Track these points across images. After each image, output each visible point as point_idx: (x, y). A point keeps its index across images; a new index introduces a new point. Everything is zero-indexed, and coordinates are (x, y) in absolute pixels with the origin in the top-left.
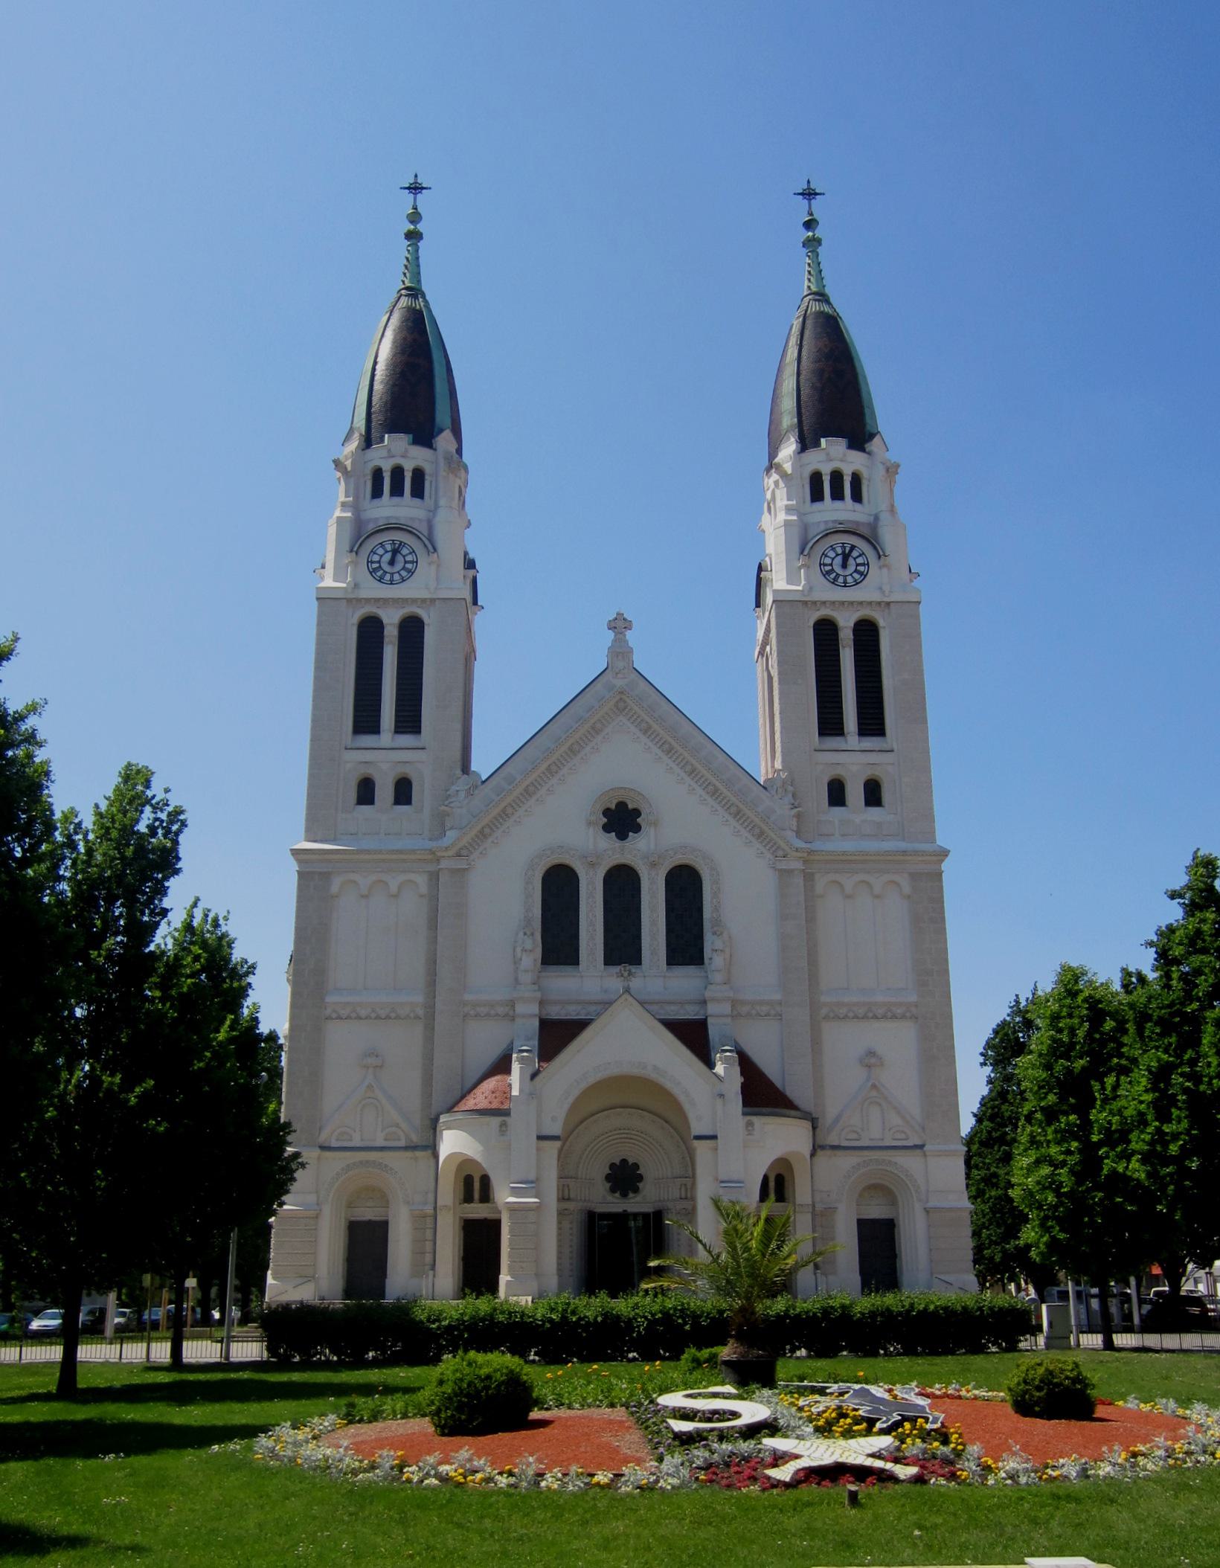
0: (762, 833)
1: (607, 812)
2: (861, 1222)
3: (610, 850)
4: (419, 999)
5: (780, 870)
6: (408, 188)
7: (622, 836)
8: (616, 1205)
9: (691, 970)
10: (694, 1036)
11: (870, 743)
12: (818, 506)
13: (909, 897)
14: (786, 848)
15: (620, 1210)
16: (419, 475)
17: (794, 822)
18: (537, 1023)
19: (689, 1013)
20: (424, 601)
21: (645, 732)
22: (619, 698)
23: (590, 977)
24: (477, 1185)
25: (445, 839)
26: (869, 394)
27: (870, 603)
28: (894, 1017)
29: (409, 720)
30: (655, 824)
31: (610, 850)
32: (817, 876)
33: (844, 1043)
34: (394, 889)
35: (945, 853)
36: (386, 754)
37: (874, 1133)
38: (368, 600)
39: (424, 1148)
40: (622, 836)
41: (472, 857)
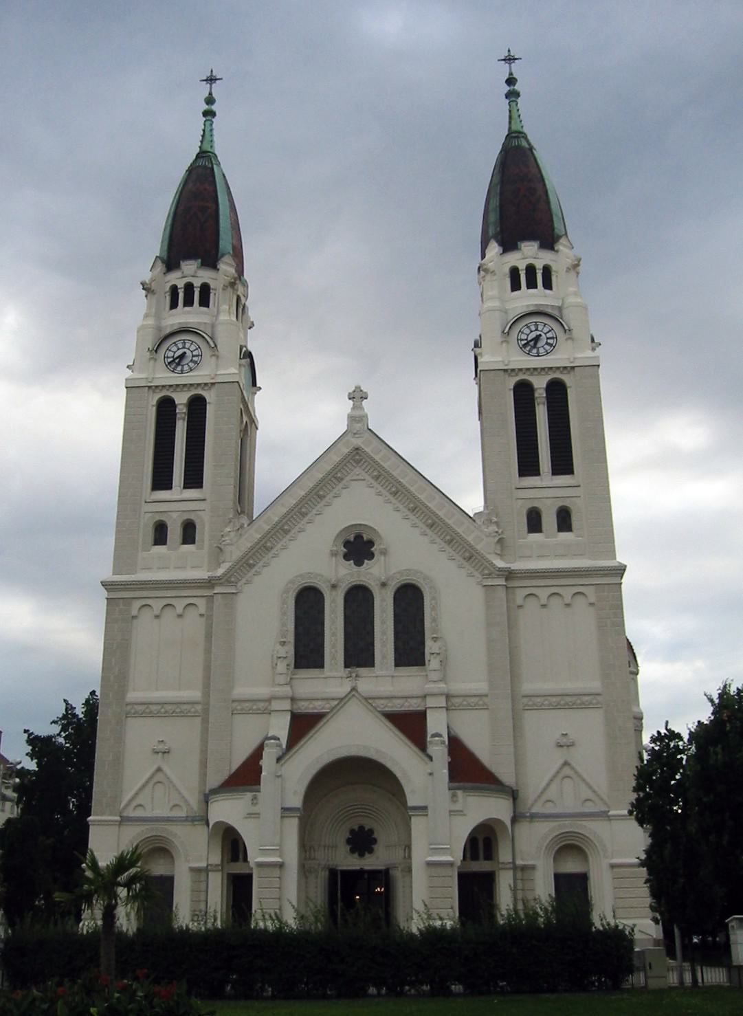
1: (347, 544)
3: (348, 574)
6: (216, 79)
7: (359, 563)
8: (353, 863)
9: (413, 670)
10: (411, 725)
15: (358, 868)
16: (547, 271)
18: (288, 717)
19: (414, 705)
22: (357, 456)
23: (329, 682)
29: (194, 478)
30: (384, 553)
31: (348, 574)
33: (543, 728)
34: (179, 610)
36: (177, 501)
37: (569, 804)
40: (359, 563)
41: (239, 584)
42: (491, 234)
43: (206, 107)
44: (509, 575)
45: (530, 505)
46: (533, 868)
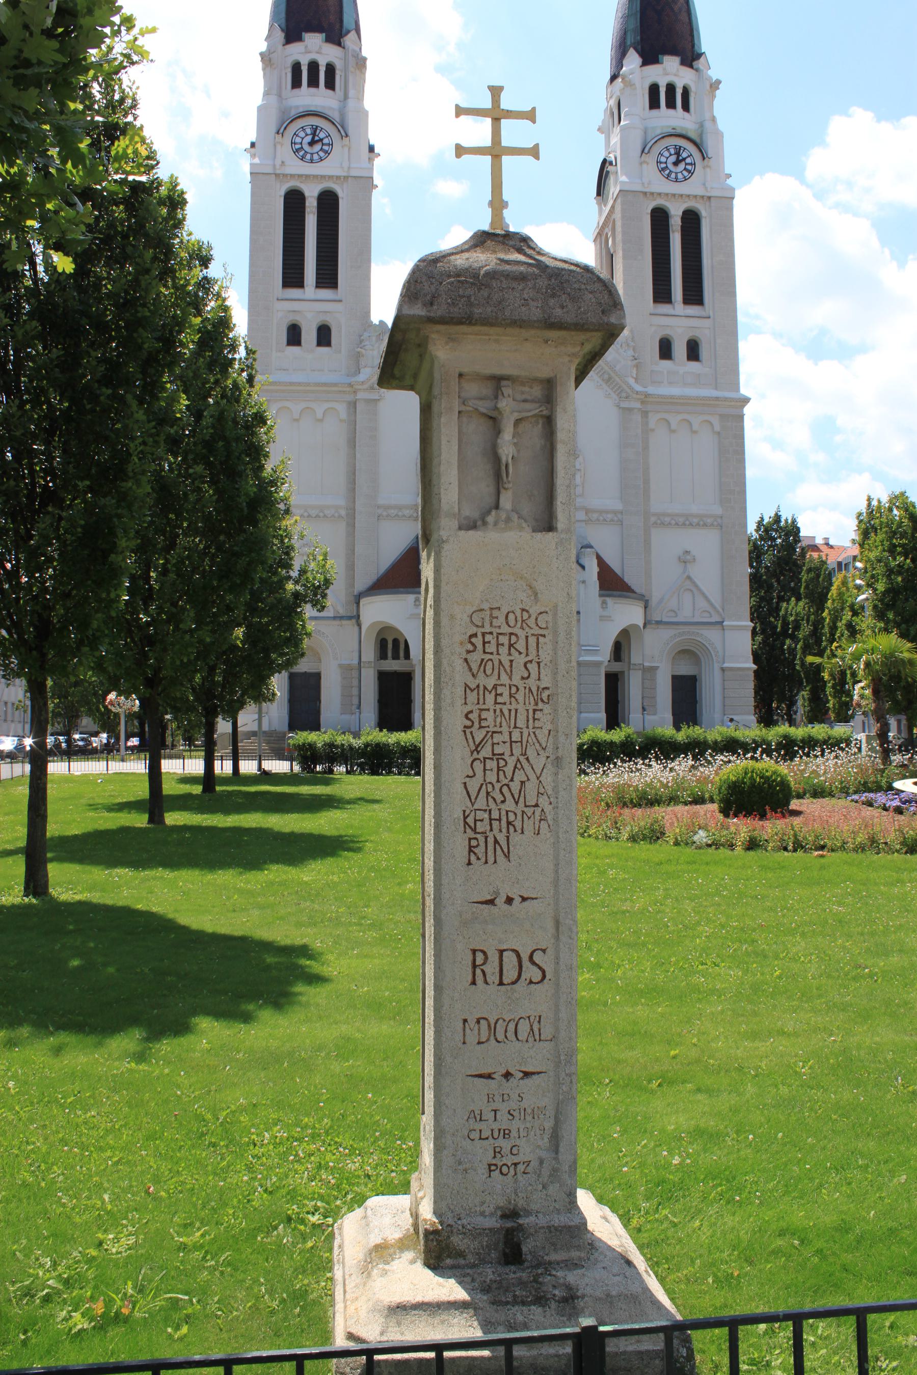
0: (610, 378)
2: (674, 678)
4: (342, 502)
5: (624, 409)
11: (693, 310)
12: (655, 112)
13: (719, 433)
14: (629, 391)
16: (331, 70)
17: (635, 371)
20: (338, 177)
24: (390, 646)
25: (361, 375)
26: (696, 18)
27: (695, 196)
28: (705, 525)
32: (650, 415)
33: (667, 544)
34: (319, 415)
35: (746, 400)
37: (686, 614)
38: (292, 176)
39: (350, 618)
42: (629, 43)
44: (645, 398)
46: (656, 668)
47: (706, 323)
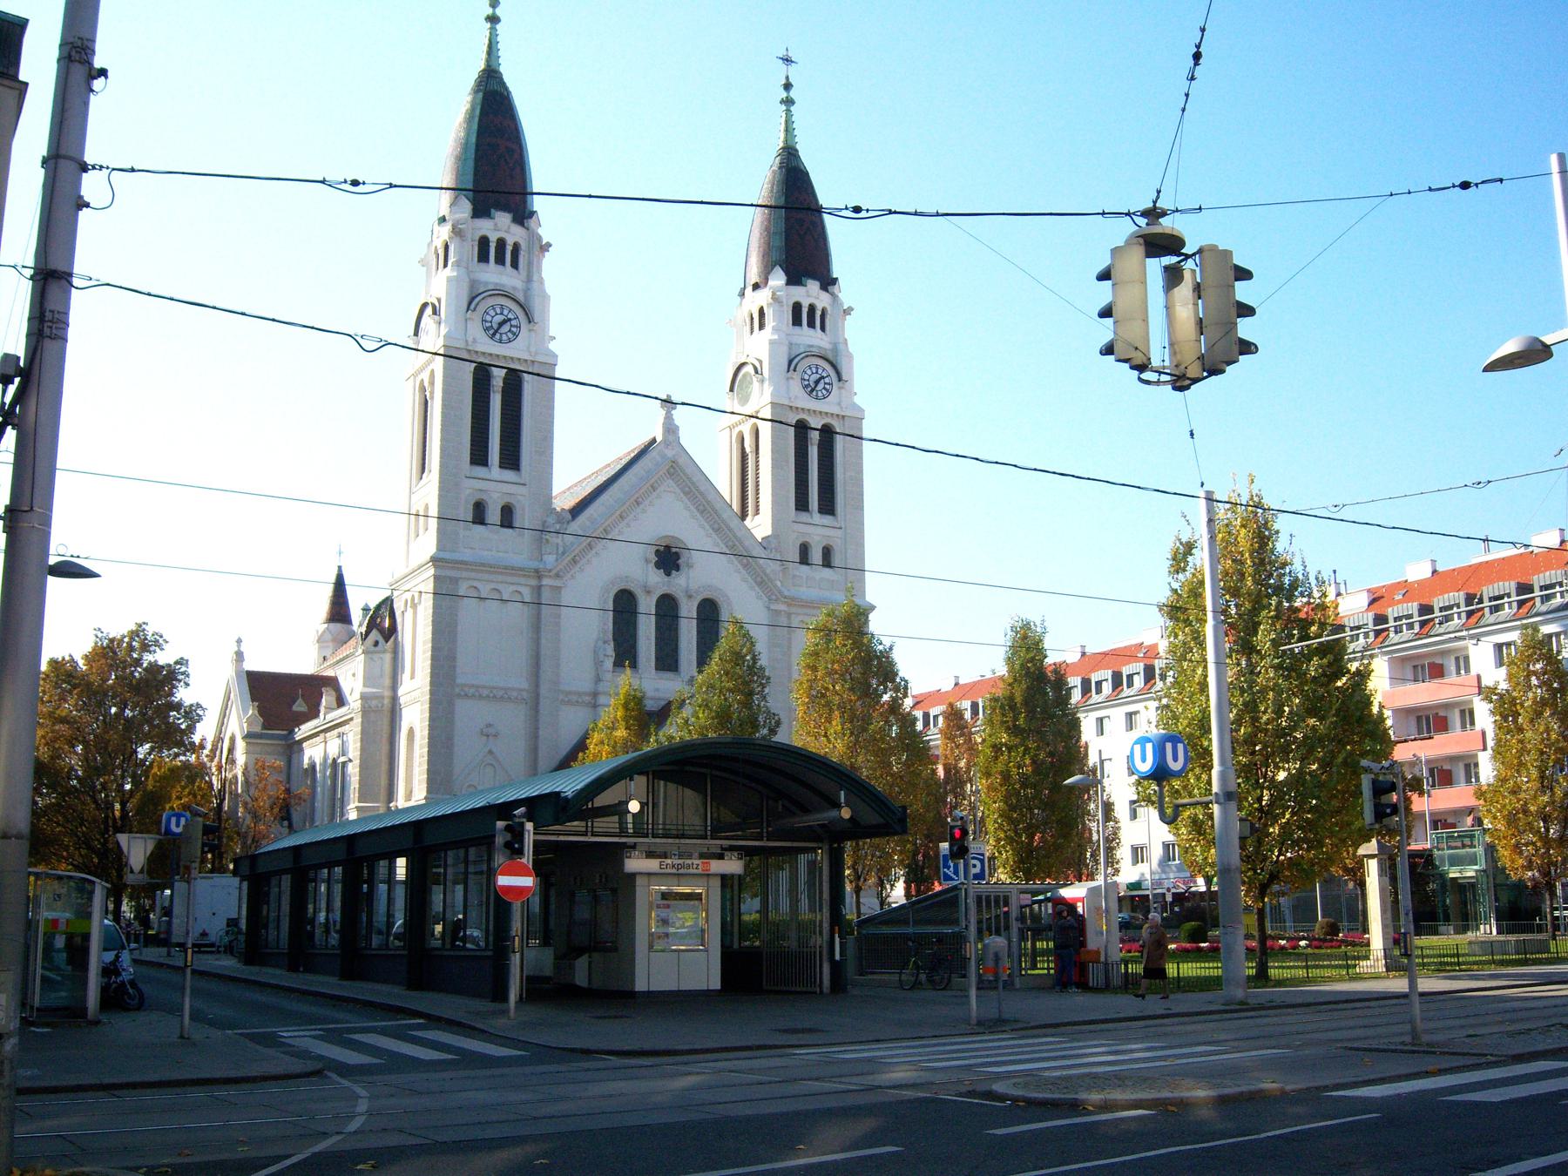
3: (657, 580)
4: (525, 685)
21: (686, 494)
22: (657, 466)
35: (873, 608)
43: (784, 95)
45: (507, 499)
47: (839, 533)
